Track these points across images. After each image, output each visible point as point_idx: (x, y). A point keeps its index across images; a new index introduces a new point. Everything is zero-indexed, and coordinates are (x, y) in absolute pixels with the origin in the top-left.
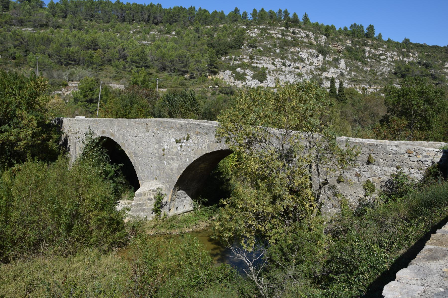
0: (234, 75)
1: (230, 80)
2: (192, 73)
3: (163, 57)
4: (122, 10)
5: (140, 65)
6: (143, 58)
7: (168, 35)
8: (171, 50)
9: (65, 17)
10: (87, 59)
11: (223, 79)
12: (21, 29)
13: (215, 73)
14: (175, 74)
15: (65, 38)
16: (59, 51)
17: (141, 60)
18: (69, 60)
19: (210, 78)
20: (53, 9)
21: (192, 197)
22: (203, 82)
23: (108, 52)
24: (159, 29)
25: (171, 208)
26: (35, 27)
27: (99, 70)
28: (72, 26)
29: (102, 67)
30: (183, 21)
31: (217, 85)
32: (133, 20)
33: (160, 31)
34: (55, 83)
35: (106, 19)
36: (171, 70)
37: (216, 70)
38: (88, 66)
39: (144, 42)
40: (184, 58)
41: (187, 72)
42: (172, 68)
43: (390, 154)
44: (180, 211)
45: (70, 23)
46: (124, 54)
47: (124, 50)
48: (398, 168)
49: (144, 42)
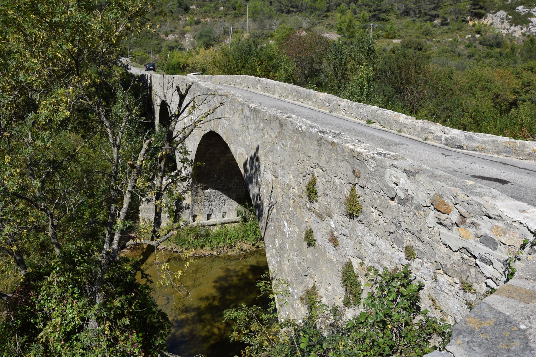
0: (510, 17)
1: (503, 26)
2: (443, 17)
5: (372, 9)
11: (492, 24)
13: (480, 16)
14: (420, 19)
18: (292, 6)
19: (471, 23)
22: (458, 29)
25: (195, 213)
27: (323, 17)
29: (328, 14)
31: (478, 32)
34: (263, 34)
37: (483, 11)
38: (312, 12)
41: (437, 16)
43: (392, 199)
44: (216, 219)
48: (410, 253)
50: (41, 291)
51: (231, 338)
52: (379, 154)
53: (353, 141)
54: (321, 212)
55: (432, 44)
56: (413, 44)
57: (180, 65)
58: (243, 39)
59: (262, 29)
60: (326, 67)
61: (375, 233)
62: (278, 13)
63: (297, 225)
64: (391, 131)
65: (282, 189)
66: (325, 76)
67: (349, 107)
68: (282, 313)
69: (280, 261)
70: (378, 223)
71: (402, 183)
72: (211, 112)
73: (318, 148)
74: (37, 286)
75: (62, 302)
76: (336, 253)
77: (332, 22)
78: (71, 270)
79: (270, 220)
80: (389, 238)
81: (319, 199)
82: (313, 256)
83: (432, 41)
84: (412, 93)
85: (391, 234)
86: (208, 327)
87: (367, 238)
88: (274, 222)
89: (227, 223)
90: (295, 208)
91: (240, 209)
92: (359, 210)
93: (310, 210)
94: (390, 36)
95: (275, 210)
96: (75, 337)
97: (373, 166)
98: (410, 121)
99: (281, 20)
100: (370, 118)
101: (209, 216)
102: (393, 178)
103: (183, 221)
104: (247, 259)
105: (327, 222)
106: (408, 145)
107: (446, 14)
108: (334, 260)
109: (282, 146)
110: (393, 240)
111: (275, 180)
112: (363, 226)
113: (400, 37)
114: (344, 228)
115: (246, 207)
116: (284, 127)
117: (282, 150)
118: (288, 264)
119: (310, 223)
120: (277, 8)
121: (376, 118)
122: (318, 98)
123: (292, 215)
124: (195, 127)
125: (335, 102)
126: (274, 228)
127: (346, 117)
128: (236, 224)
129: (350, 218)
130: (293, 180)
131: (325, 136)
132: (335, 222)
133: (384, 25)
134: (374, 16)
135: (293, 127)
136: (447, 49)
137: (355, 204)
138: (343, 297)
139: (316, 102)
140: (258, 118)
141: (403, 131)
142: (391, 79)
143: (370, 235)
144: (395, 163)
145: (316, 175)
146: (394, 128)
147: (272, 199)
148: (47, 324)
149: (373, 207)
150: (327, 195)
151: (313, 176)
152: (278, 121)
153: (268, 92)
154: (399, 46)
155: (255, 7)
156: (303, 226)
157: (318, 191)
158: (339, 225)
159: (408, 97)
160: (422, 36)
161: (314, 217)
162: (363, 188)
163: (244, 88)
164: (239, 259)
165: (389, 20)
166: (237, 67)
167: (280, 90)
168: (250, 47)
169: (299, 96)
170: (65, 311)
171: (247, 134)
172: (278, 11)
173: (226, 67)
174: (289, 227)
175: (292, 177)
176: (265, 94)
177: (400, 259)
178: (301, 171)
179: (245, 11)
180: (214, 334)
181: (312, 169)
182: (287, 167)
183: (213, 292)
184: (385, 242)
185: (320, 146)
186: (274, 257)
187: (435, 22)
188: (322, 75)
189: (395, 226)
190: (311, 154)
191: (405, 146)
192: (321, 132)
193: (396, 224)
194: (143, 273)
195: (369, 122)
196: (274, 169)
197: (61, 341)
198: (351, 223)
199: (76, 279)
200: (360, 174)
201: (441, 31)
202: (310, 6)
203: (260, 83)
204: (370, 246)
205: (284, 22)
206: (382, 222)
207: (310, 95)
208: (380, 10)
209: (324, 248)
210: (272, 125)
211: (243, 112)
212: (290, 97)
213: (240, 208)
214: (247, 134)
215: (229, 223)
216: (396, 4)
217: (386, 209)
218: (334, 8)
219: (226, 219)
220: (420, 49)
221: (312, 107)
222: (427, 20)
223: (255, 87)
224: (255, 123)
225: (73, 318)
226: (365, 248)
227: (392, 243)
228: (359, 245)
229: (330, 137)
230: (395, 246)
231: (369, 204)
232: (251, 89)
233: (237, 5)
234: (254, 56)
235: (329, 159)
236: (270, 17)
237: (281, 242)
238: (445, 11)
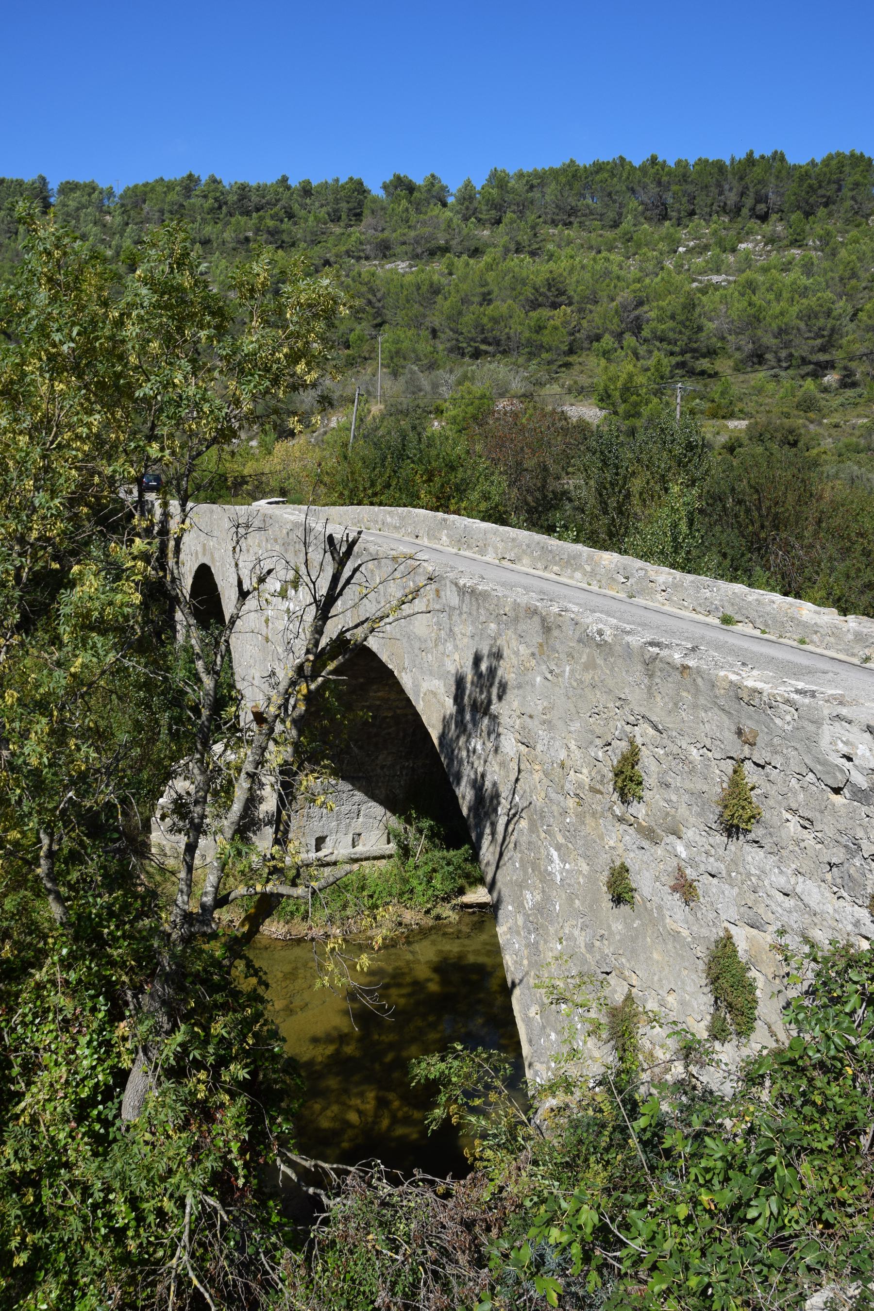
2: (845, 368)
3: (756, 320)
4: (659, 183)
5: (677, 349)
6: (686, 327)
7: (795, 251)
8: (785, 295)
9: (498, 222)
10: (527, 334)
12: (382, 267)
14: (791, 372)
15: (477, 279)
16: (455, 316)
17: (680, 332)
18: (485, 341)
20: (467, 203)
21: (392, 805)
23: (591, 312)
24: (768, 234)
26: (416, 257)
27: (560, 366)
28: (513, 246)
29: (571, 359)
30: (853, 198)
32: (692, 213)
33: (770, 240)
34: (418, 406)
35: (611, 215)
36: (779, 360)
38: (531, 355)
39: (715, 278)
40: (821, 322)
41: (829, 365)
42: (783, 354)
43: (837, 791)
45: (506, 238)
46: (637, 318)
47: (640, 303)
49: (715, 278)
50: (18, 1004)
51: (429, 1125)
52: (798, 692)
53: (732, 666)
54: (653, 824)
55: (821, 430)
56: (776, 431)
57: (226, 480)
58: (370, 418)
59: (414, 393)
60: (580, 487)
61: (794, 866)
62: (452, 355)
63: (586, 857)
64: (782, 640)
65: (546, 774)
66: (576, 509)
67: (676, 586)
68: (538, 1066)
69: (537, 942)
70: (802, 845)
71: (863, 756)
72: (410, 597)
73: (646, 681)
74: (9, 993)
75: (68, 1031)
76: (691, 918)
77: (584, 380)
78: (93, 955)
79: (512, 845)
80: (829, 876)
81: (647, 795)
82: (629, 927)
83: (820, 424)
84: (787, 547)
85: (834, 869)
86: (335, 1108)
87: (773, 878)
88: (521, 852)
89: (361, 860)
90: (581, 817)
91: (396, 826)
92: (754, 817)
93: (621, 820)
94: (721, 413)
95: (523, 824)
96: (95, 1112)
97: (788, 718)
98: (826, 618)
99: (459, 372)
100: (729, 611)
101: (320, 842)
102: (841, 745)
103: (258, 854)
104: (416, 947)
105: (669, 848)
106: (836, 674)
107: (851, 359)
108: (685, 933)
109: (549, 676)
110: (839, 881)
111: (528, 754)
112: (761, 853)
113: (744, 414)
114: (712, 859)
115: (408, 821)
116: (556, 633)
117: (547, 683)
118: (559, 947)
119: (620, 851)
120: (448, 345)
121: (744, 612)
122: (597, 564)
123: (571, 833)
124: (371, 632)
125: (642, 573)
126: (522, 865)
127: (668, 608)
128: (384, 861)
129: (729, 836)
130: (577, 754)
131: (664, 653)
132: (687, 847)
133: (706, 386)
134: (682, 365)
135: (578, 634)
136: (858, 445)
137: (744, 803)
138: (709, 1017)
139: (593, 574)
140: (482, 611)
141: (812, 642)
142: (736, 516)
143: (781, 872)
144: (844, 711)
145: (639, 741)
146: (788, 635)
147: (517, 798)
148: (34, 1083)
149: (789, 809)
150: (668, 786)
151: (632, 743)
152: (536, 619)
153: (469, 547)
154: (743, 435)
155: (397, 341)
156: (604, 859)
157: (645, 778)
158: (699, 853)
159: (777, 557)
160: (796, 412)
161: (631, 836)
162: (763, 767)
163: (406, 538)
164: (393, 946)
165: (716, 374)
166: (373, 485)
167: (500, 545)
168: (404, 439)
169: (548, 558)
170: (74, 1052)
171: (450, 646)
172: (451, 350)
173: (347, 485)
174: (563, 861)
175: (573, 747)
176: (461, 552)
177: (857, 924)
178: (598, 731)
179: (373, 350)
180: (348, 1124)
181: (628, 728)
182: (560, 724)
183: (344, 1024)
184: (819, 886)
185: (651, 676)
186: (518, 933)
187: (826, 379)
188: (568, 506)
189: (843, 850)
190: (626, 693)
191: (831, 674)
192: (651, 644)
193: (846, 846)
194: (249, 965)
195: (727, 620)
196: (524, 728)
197: (68, 1121)
198: (732, 847)
199: (105, 977)
200: (755, 737)
201: (840, 400)
202: (528, 340)
203: (447, 528)
204: (780, 897)
205: (465, 377)
206: (813, 842)
207: (577, 556)
208: (694, 350)
209: (660, 908)
210: (522, 627)
211: (438, 596)
212: (526, 560)
213: (395, 822)
214: (450, 646)
215: (367, 859)
216: (731, 338)
217: (822, 812)
218: (586, 345)
219: (361, 849)
220: (794, 444)
221: (585, 586)
222: (808, 374)
223: (432, 536)
224: (473, 623)
225: (93, 1068)
226: (768, 902)
227: (835, 889)
228: (753, 896)
229: (676, 656)
230: (845, 895)
231: (779, 803)
232: (425, 541)
233: (352, 337)
234: (413, 462)
235: (676, 704)
236: (432, 366)
237: (538, 898)
238: (848, 353)
